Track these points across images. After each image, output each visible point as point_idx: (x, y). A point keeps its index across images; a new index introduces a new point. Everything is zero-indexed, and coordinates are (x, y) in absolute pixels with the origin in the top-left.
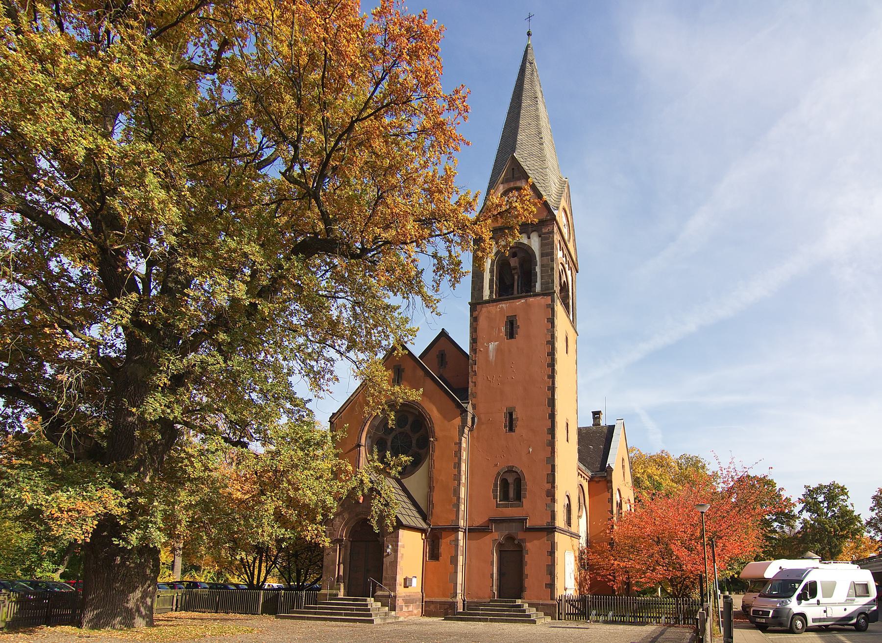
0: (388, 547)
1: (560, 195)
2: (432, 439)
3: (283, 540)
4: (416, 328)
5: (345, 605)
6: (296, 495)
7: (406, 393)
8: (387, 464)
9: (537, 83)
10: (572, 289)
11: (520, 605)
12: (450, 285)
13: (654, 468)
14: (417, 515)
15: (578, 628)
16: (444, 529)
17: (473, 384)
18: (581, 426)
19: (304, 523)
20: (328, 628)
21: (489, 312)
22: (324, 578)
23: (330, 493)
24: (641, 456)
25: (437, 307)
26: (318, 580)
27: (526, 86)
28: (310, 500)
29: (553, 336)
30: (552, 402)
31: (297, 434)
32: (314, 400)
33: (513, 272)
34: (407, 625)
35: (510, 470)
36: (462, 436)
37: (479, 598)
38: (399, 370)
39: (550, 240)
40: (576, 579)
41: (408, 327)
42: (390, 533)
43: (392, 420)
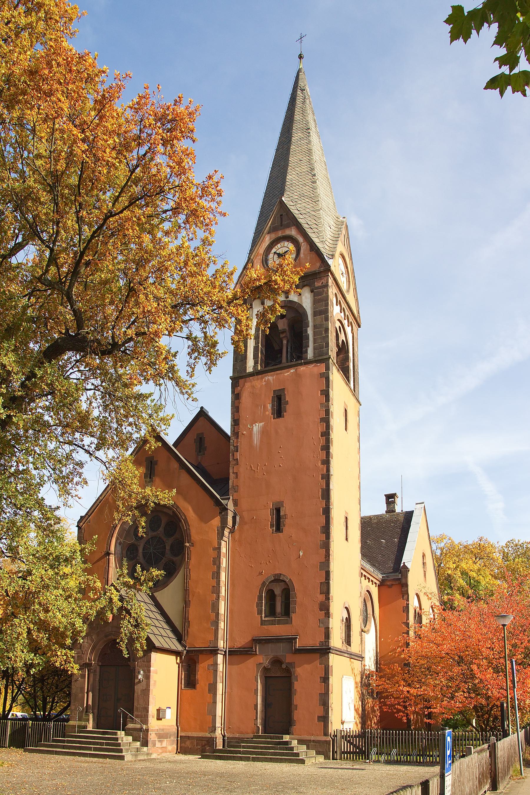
0: (139, 673)
1: (336, 239)
2: (187, 544)
3: (32, 665)
4: (171, 416)
5: (94, 738)
6: (46, 617)
7: (157, 496)
8: (137, 579)
9: (309, 111)
10: (353, 348)
11: (287, 742)
12: (206, 369)
13: (471, 562)
14: (171, 635)
15: (353, 769)
16: (201, 652)
17: (234, 475)
18: (362, 516)
19: (53, 648)
20: (77, 764)
21: (253, 387)
22: (72, 707)
23: (79, 615)
24: (452, 546)
25: (192, 393)
26: (65, 709)
27: (297, 117)
28: (60, 623)
29: (327, 412)
30: (326, 494)
31: (48, 550)
32: (62, 508)
33: (281, 336)
34: (160, 762)
35: (277, 579)
36: (222, 539)
37: (242, 733)
38: (151, 462)
39: (324, 295)
40: (356, 710)
41: (161, 415)
42: (140, 658)
43: (143, 528)
